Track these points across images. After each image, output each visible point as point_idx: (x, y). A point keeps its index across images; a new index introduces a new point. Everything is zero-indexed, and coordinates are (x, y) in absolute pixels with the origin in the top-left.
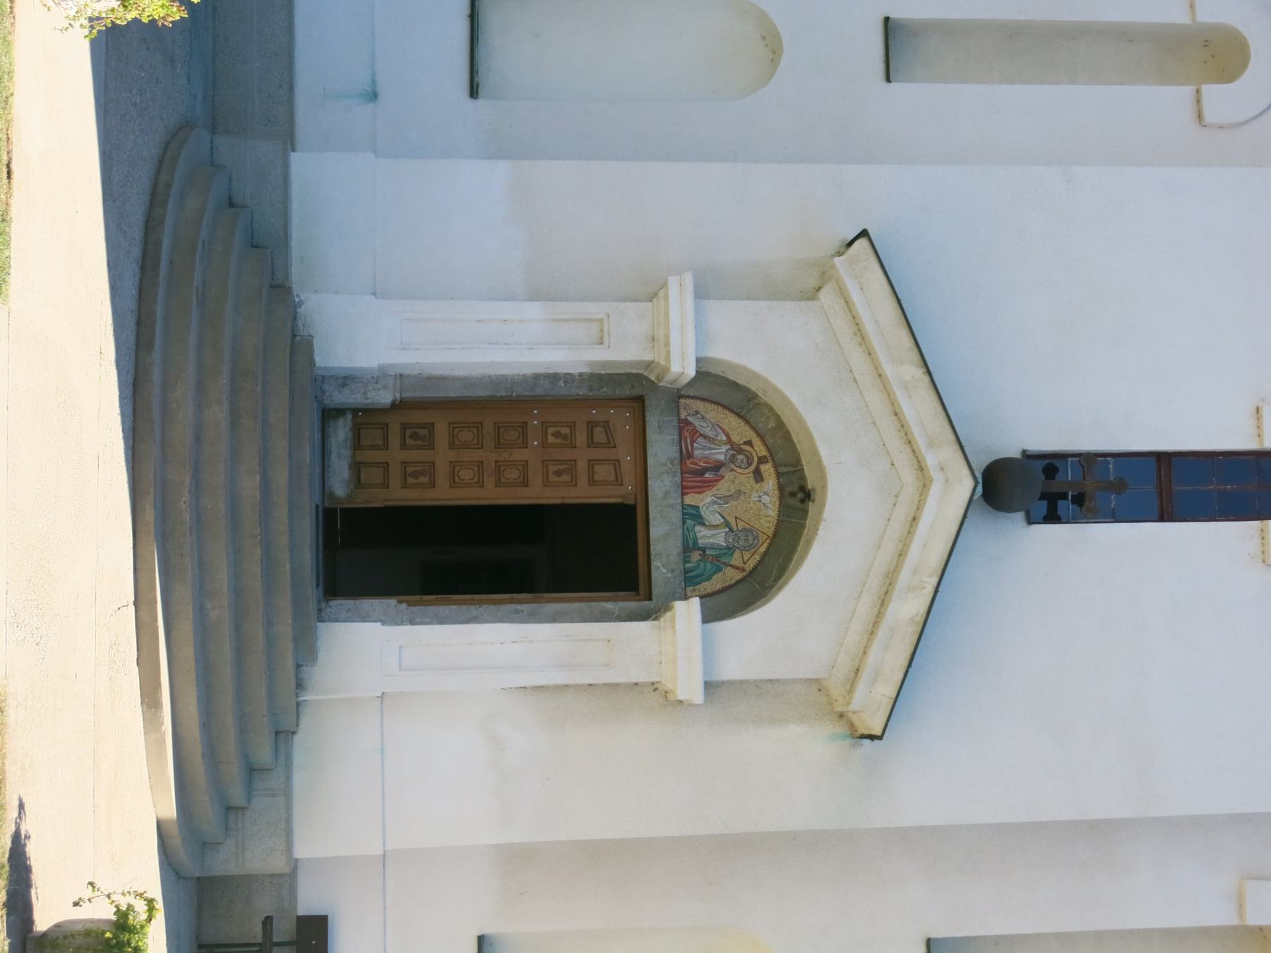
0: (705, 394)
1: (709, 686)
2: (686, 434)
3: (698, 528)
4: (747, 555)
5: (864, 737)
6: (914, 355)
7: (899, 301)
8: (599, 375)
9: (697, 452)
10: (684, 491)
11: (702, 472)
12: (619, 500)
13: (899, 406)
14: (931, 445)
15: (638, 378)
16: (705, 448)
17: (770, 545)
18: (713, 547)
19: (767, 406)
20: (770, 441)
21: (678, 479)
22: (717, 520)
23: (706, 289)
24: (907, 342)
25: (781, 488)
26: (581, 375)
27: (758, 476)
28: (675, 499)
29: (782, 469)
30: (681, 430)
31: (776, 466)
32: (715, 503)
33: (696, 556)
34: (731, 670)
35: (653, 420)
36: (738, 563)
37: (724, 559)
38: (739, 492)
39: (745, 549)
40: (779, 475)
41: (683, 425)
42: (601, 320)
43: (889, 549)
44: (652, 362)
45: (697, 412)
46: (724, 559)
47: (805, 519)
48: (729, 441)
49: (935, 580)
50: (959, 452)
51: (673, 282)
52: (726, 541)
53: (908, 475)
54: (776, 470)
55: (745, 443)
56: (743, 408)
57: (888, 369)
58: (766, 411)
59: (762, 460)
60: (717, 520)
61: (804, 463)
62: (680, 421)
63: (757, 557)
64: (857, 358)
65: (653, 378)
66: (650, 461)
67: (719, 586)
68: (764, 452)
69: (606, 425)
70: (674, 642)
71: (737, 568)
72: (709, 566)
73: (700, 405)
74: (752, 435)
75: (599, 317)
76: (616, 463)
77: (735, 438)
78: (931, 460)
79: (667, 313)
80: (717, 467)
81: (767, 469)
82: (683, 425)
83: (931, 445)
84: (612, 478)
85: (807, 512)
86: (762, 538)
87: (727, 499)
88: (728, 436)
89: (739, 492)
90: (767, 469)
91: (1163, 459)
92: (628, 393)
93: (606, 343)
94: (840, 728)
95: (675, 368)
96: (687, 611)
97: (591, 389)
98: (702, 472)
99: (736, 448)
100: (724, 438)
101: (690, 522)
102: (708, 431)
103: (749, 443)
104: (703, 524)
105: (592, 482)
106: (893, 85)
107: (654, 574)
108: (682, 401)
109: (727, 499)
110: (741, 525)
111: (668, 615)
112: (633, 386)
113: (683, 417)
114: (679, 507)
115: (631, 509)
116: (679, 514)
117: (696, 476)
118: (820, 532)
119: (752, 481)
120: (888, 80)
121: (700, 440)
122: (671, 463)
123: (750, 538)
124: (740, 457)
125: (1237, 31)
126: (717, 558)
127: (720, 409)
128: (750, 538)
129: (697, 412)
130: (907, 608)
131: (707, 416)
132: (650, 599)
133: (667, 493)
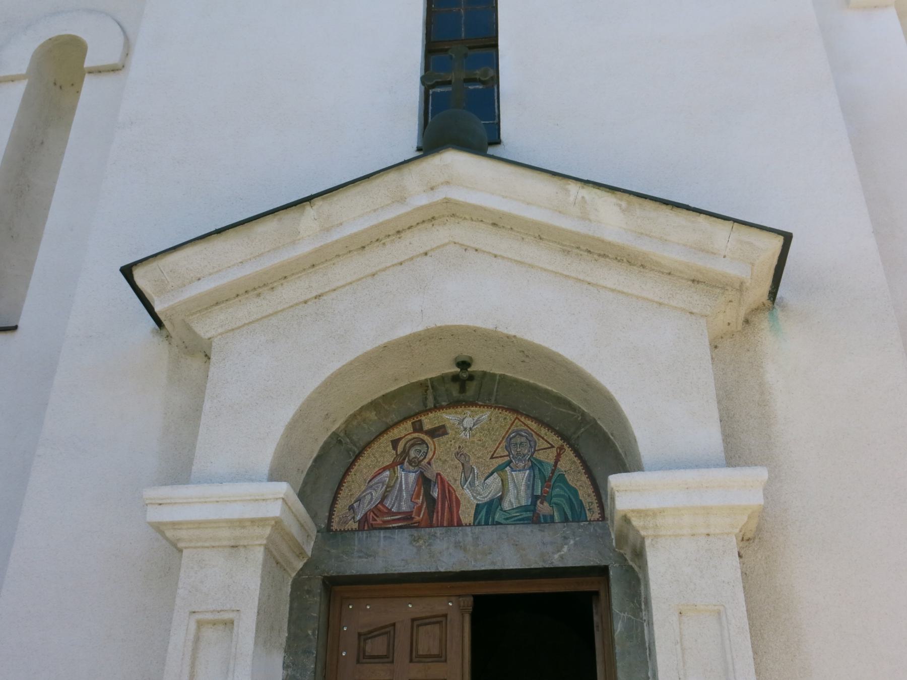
0: (328, 496)
1: (734, 455)
2: (379, 521)
3: (506, 506)
4: (542, 444)
5: (773, 294)
6: (288, 217)
8: (288, 638)
9: (404, 508)
10: (454, 522)
11: (431, 502)
12: (467, 618)
13: (352, 237)
14: (402, 200)
15: (297, 585)
16: (399, 497)
17: (527, 416)
18: (531, 486)
19: (348, 422)
20: (394, 417)
21: (439, 531)
22: (494, 482)
23: (179, 470)
24: (269, 226)
25: (455, 404)
26: (286, 667)
27: (438, 432)
28: (467, 535)
29: (430, 404)
30: (373, 528)
31: (426, 411)
32: (472, 484)
33: (544, 508)
34: (709, 437)
35: (358, 565)
36: (553, 453)
37: (548, 473)
38: (458, 454)
40: (437, 407)
41: (366, 525)
42: (200, 624)
43: (531, 252)
44: (267, 549)
45: (351, 507)
46: (548, 473)
47: (494, 375)
48: (391, 467)
49: (573, 187)
51: (156, 515)
52: (524, 469)
53: (440, 234)
54: (431, 410)
55: (395, 447)
57: (304, 248)
58: (355, 423)
59: (418, 427)
60: (494, 482)
61: (423, 378)
62: (361, 529)
63: (543, 431)
64: (290, 292)
65: (299, 565)
66: (414, 568)
67: (584, 478)
68: (408, 425)
69: (363, 637)
70: (674, 507)
71: (558, 456)
72: (557, 491)
74: (386, 439)
75: (193, 626)
76: (417, 622)
77: (388, 460)
79: (199, 524)
80: (425, 482)
81: (429, 421)
82: (366, 525)
83: (402, 200)
84: (436, 628)
85: (484, 374)
86: (518, 425)
87: (467, 470)
88: (385, 469)
89: (458, 454)
90: (429, 421)
91: (432, 48)
92: (317, 599)
93: (231, 616)
94: (763, 323)
95: (275, 510)
97: (307, 652)
98: (431, 502)
99: (401, 460)
100: (388, 473)
101: (497, 517)
102: (377, 495)
103: (395, 443)
104: (501, 499)
105: (440, 657)
106: (21, 324)
107: (570, 563)
108: (335, 526)
109: (467, 470)
110: (502, 451)
111: (636, 522)
112: (308, 592)
113: (355, 526)
114: (477, 529)
115: (479, 600)
116: (488, 529)
117: (435, 507)
118: (512, 332)
119: (444, 438)
120: (15, 328)
121: (388, 503)
122: (416, 540)
123: (519, 440)
124: (412, 454)
125: (42, 46)
126: (546, 481)
127: (349, 478)
128: (519, 440)
129: (351, 507)
130: (610, 219)
131: (356, 496)
132: (603, 571)
133: (457, 545)
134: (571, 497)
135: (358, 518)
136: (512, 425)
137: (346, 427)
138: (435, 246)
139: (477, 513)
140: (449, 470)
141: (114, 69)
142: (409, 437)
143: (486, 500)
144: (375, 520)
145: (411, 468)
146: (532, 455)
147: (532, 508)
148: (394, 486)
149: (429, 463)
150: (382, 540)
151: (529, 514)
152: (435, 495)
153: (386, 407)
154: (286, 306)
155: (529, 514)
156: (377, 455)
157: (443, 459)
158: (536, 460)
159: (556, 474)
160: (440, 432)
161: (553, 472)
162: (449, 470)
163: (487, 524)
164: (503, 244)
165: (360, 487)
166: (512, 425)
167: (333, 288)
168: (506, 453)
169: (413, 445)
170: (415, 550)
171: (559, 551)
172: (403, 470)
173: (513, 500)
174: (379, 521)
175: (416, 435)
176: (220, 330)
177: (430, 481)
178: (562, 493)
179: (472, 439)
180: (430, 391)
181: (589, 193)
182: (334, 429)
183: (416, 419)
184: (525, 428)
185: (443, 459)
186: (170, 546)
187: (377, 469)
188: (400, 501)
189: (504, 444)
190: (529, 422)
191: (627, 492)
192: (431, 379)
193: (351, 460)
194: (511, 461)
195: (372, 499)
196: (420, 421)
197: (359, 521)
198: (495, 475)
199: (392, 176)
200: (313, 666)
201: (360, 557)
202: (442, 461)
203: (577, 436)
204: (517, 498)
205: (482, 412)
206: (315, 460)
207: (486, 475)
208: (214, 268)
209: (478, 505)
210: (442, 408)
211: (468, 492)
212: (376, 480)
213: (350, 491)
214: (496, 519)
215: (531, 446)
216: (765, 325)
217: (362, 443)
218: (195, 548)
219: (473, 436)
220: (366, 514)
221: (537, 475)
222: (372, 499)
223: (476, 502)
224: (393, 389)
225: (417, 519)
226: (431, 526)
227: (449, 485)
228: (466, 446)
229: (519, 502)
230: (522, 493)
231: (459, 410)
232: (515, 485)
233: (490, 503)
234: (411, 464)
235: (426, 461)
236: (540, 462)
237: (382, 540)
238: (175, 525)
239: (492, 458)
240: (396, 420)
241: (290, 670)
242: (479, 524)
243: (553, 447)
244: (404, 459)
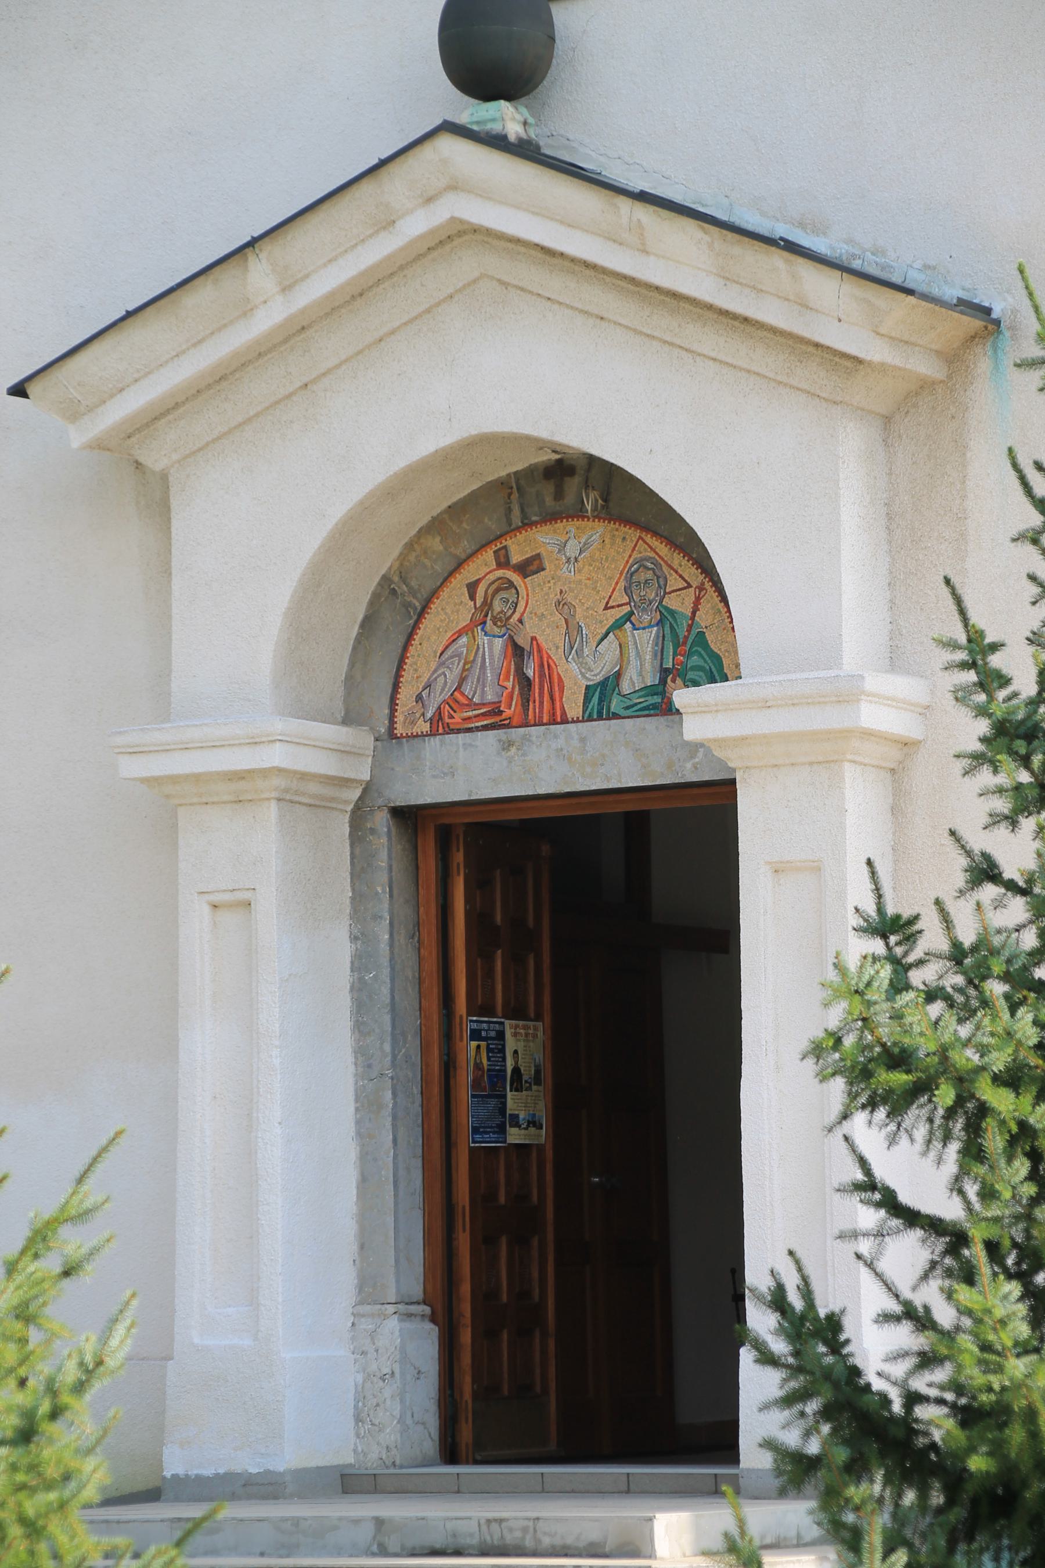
3: (626, 687)
6: (226, 275)
7: (129, 314)
9: (490, 697)
11: (526, 683)
16: (481, 680)
17: (655, 534)
18: (660, 654)
19: (402, 557)
24: (203, 294)
25: (551, 517)
27: (530, 567)
29: (517, 521)
31: (512, 530)
32: (579, 653)
36: (690, 595)
39: (661, 581)
40: (527, 524)
46: (682, 632)
49: (625, 205)
50: (392, 167)
52: (650, 626)
53: (467, 264)
54: (518, 529)
55: (472, 597)
56: (407, 605)
58: (412, 557)
59: (503, 561)
61: (503, 473)
62: (433, 734)
68: (488, 556)
72: (695, 660)
77: (464, 620)
78: (417, 224)
80: (517, 652)
81: (518, 549)
87: (573, 630)
88: (460, 634)
90: (518, 549)
92: (384, 840)
96: (708, 717)
98: (526, 683)
100: (464, 640)
101: (616, 704)
102: (452, 676)
103: (472, 588)
104: (618, 675)
108: (399, 730)
109: (573, 630)
121: (467, 690)
124: (497, 605)
127: (412, 651)
128: (643, 576)
131: (424, 680)
134: (713, 669)
135: (429, 715)
136: (633, 549)
137: (401, 564)
138: (461, 285)
139: (587, 699)
140: (548, 631)
142: (491, 577)
143: (599, 678)
144: (451, 717)
145: (496, 630)
146: (661, 602)
147: (661, 688)
148: (474, 661)
149: (520, 621)
150: (461, 749)
151: (657, 699)
152: (530, 673)
153: (454, 528)
154: (259, 409)
155: (657, 699)
156: (449, 611)
157: (539, 613)
158: (666, 608)
159: (694, 632)
160: (534, 567)
161: (690, 628)
162: (548, 631)
163: (600, 718)
164: (555, 284)
165: (428, 662)
166: (633, 549)
167: (322, 371)
168: (626, 599)
169: (497, 590)
170: (505, 763)
171: (692, 757)
172: (486, 634)
173: (635, 678)
174: (458, 717)
175: (500, 573)
176: (175, 457)
177: (522, 649)
178: (701, 663)
179: (578, 577)
180: (515, 495)
181: (643, 213)
182: (383, 572)
183: (499, 546)
184: (652, 554)
185: (539, 613)
187: (449, 634)
188: (484, 686)
189: (622, 584)
190: (655, 543)
192: (516, 473)
193: (412, 622)
194: (632, 613)
195: (446, 682)
196: (505, 547)
197: (431, 719)
198: (611, 634)
199: (366, 187)
200: (387, 937)
201: (434, 777)
202: (541, 627)
204: (640, 674)
205: (592, 528)
206: (363, 625)
207: (599, 637)
208: (138, 371)
209: (587, 687)
210: (531, 524)
211: (574, 666)
212: (449, 652)
213: (416, 670)
214: (612, 710)
215: (660, 587)
217: (425, 593)
218: (191, 804)
219: (580, 571)
220: (439, 708)
221: (668, 636)
222: (446, 682)
223: (585, 683)
224: (462, 495)
225: (508, 713)
226: (526, 725)
227: (549, 657)
228: (571, 590)
229: (643, 681)
230: (648, 666)
231: (559, 525)
232: (638, 654)
233: (603, 684)
234: (495, 624)
235: (516, 616)
236: (672, 613)
237: (461, 749)
239: (606, 608)
240: (469, 551)
241: (359, 943)
242: (590, 719)
243: (689, 586)
244: (486, 616)
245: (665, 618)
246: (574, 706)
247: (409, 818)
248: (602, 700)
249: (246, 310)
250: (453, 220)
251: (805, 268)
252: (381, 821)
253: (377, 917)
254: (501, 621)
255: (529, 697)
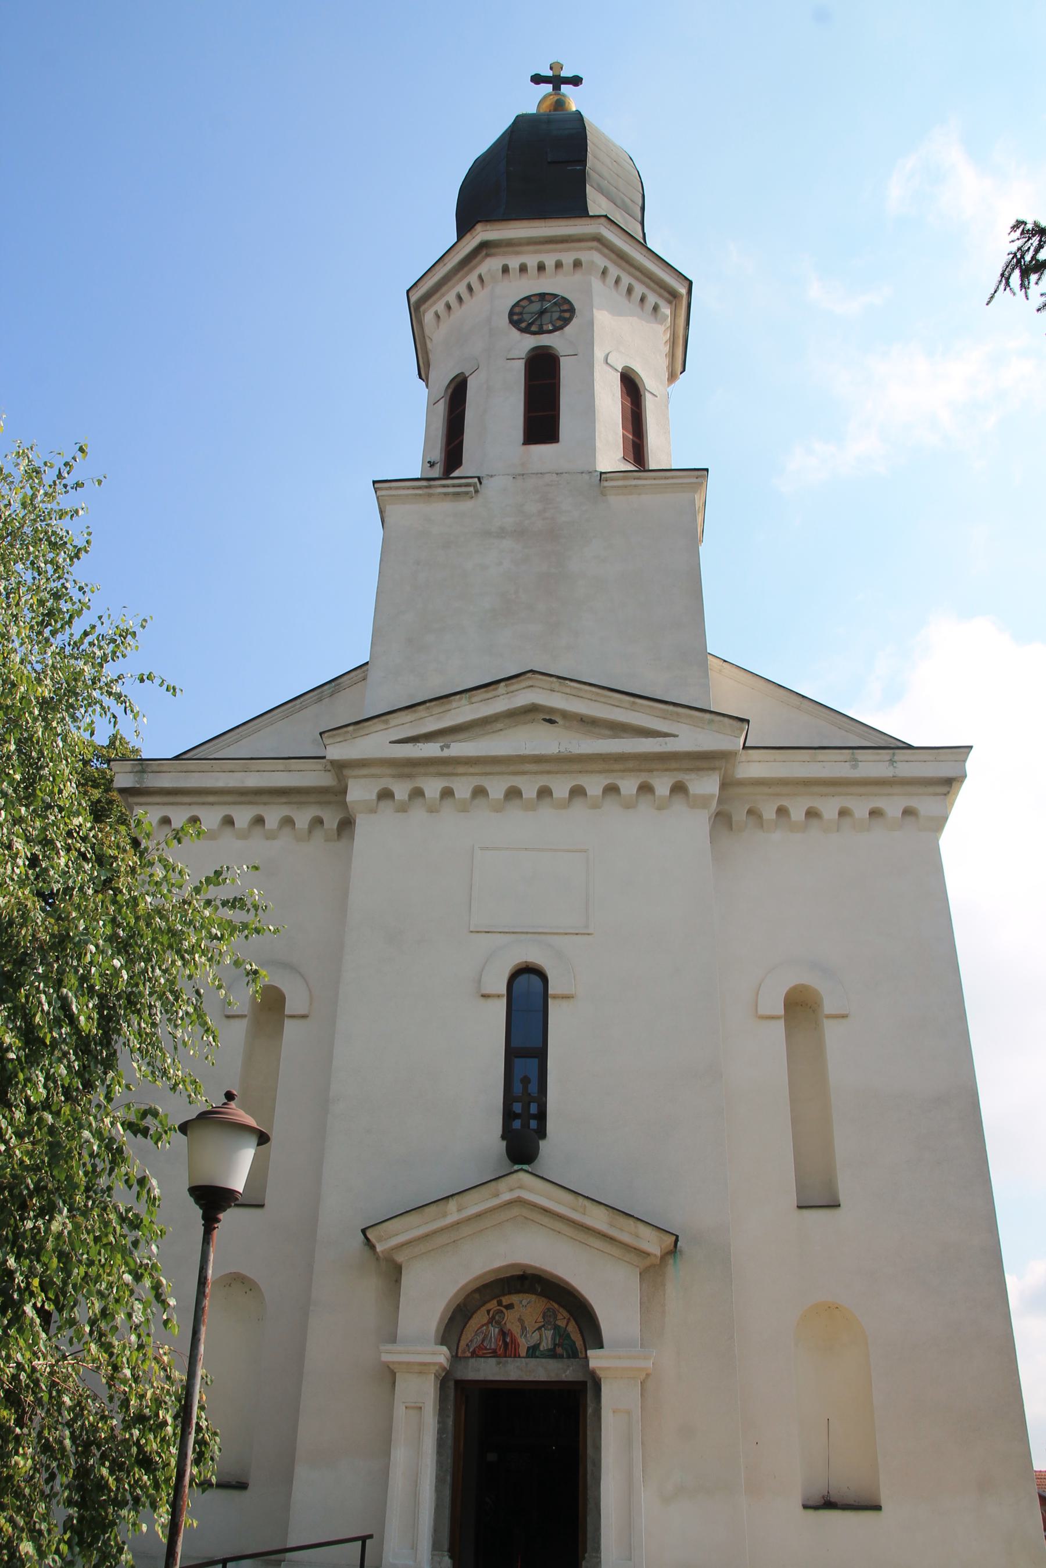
3: (542, 1348)
9: (493, 1346)
22: (536, 1335)
24: (433, 1209)
25: (518, 1292)
27: (510, 1307)
31: (504, 1295)
33: (559, 1350)
40: (510, 1293)
49: (581, 1200)
53: (516, 1211)
59: (500, 1303)
60: (536, 1335)
68: (495, 1302)
73: (463, 1344)
74: (484, 1309)
77: (485, 1320)
78: (507, 1197)
80: (503, 1333)
81: (506, 1300)
87: (524, 1328)
98: (506, 1344)
99: (491, 1321)
101: (537, 1353)
102: (480, 1338)
103: (488, 1312)
104: (539, 1344)
108: (460, 1354)
109: (524, 1328)
124: (497, 1318)
126: (560, 1336)
141: (304, 1017)
164: (546, 1220)
181: (587, 1203)
186: (389, 1375)
191: (596, 1359)
199: (493, 1183)
203: (575, 1318)
216: (671, 1261)
238: (393, 1363)
245: (556, 1328)
246: (523, 1353)
247: (462, 1386)
248: (533, 1352)
249: (445, 1215)
250: (519, 1197)
251: (640, 1225)
252: (452, 1384)
253: (448, 1416)
254: (498, 1323)
255: (507, 1348)
